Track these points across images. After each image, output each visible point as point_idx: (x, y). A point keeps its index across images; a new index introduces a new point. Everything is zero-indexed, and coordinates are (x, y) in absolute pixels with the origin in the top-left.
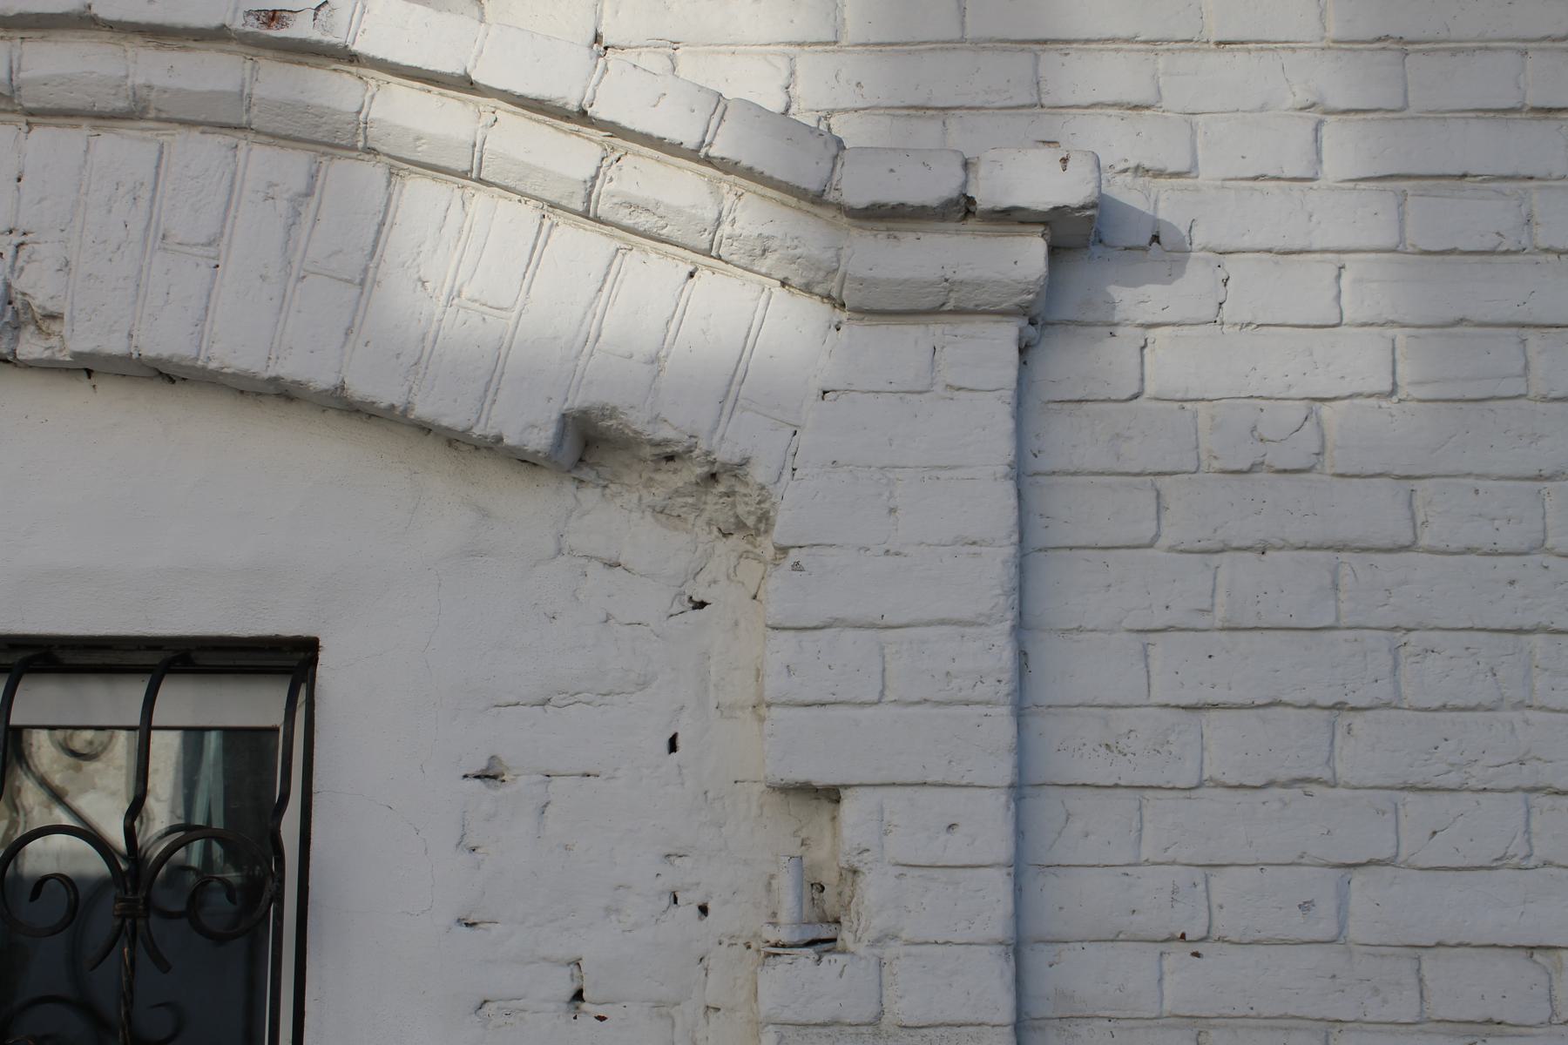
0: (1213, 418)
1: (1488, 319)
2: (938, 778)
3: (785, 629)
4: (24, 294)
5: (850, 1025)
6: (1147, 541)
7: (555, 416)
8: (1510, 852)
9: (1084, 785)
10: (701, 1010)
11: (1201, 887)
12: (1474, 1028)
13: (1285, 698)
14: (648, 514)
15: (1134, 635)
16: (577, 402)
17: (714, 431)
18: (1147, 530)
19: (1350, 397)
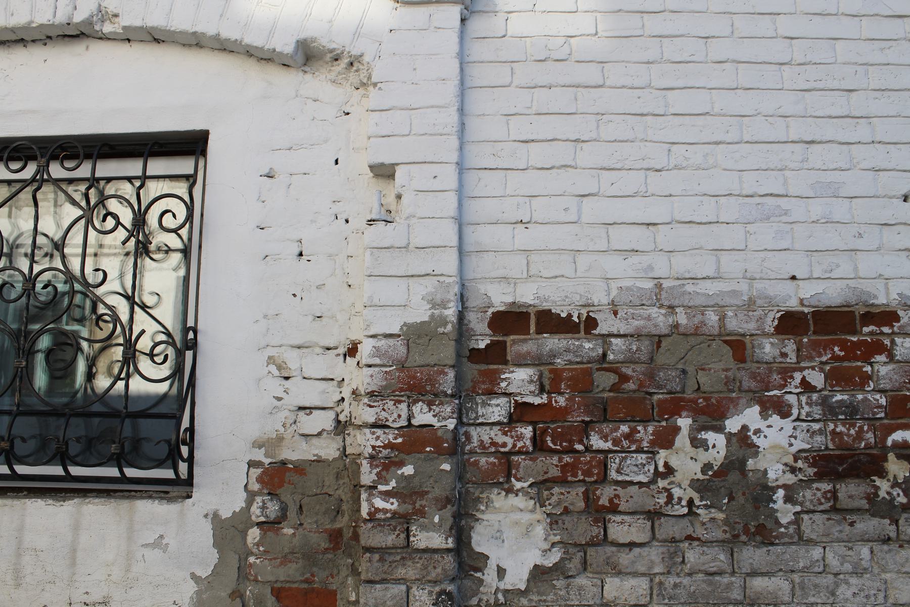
0: (532, 42)
1: (629, 10)
2: (430, 160)
3: (375, 111)
4: (106, 8)
5: (398, 248)
6: (507, 84)
7: (294, 41)
8: (640, 190)
9: (486, 169)
10: (346, 257)
11: (528, 203)
12: (628, 253)
13: (559, 137)
14: (329, 82)
15: (504, 117)
16: (302, 36)
17: (351, 44)
18: (507, 80)
19: (580, 35)
